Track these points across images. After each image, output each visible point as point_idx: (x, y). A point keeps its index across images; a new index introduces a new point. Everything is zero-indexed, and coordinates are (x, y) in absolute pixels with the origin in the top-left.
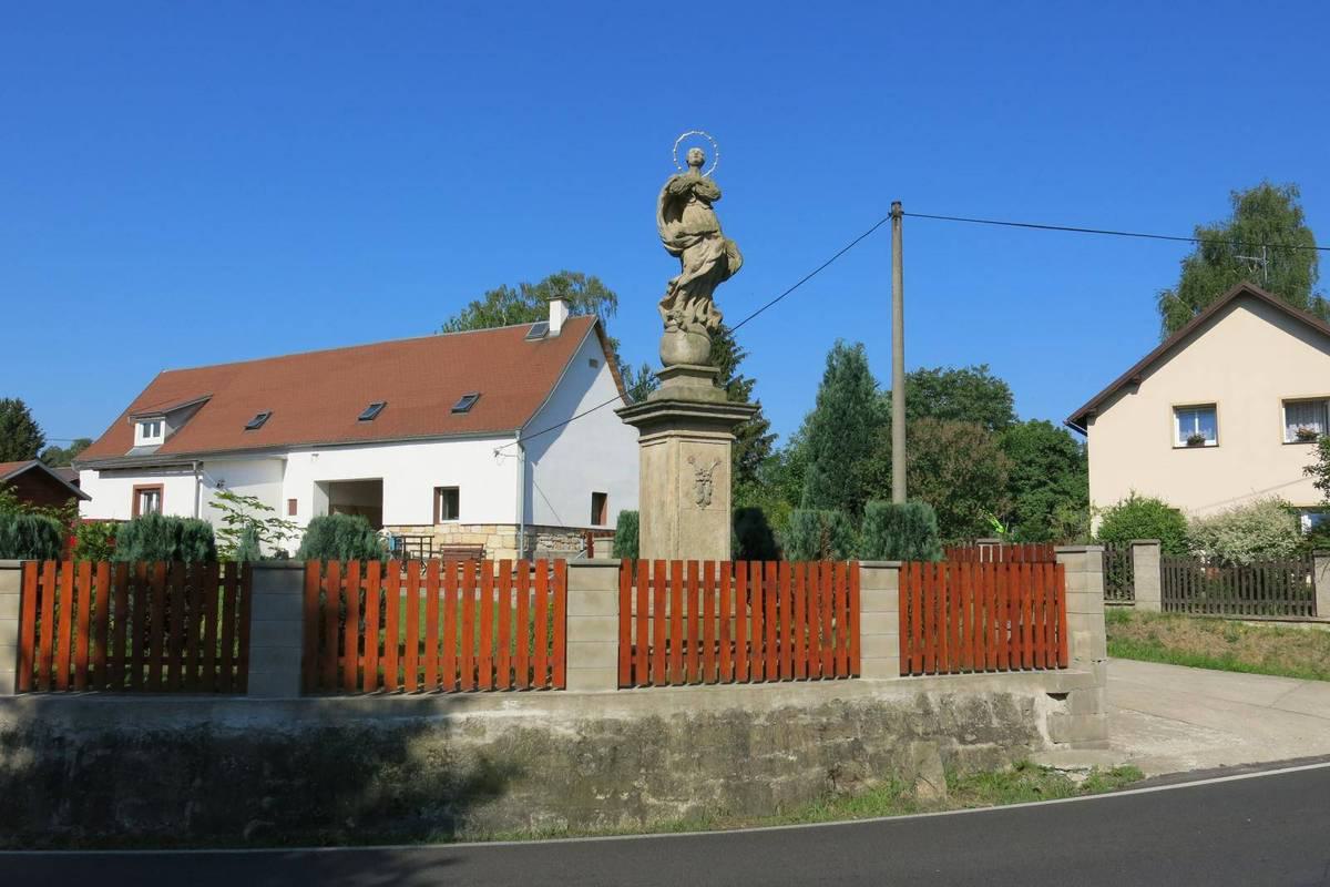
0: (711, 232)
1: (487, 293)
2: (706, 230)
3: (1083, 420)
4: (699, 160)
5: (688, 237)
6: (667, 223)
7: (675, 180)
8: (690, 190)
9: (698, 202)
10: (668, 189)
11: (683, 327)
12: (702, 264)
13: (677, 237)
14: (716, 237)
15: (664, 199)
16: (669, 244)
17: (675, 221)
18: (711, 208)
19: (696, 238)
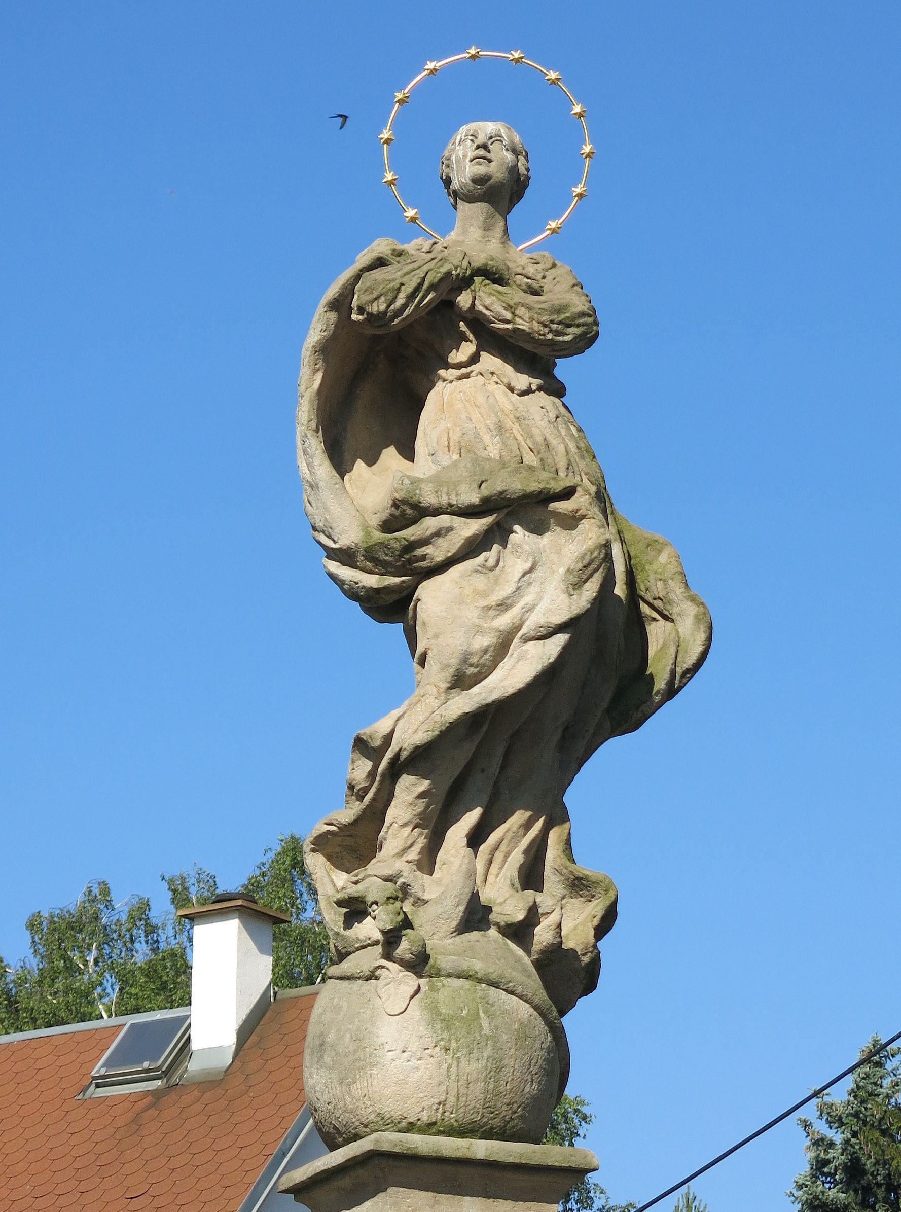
0: (545, 498)
1: (33, 925)
2: (517, 485)
3: (330, 978)
4: (496, 170)
5: (430, 524)
6: (341, 466)
7: (380, 263)
8: (446, 305)
9: (489, 361)
10: (340, 304)
11: (404, 948)
12: (502, 649)
13: (388, 526)
14: (571, 522)
15: (325, 349)
16: (346, 556)
17: (390, 456)
18: (556, 389)
19: (473, 527)
